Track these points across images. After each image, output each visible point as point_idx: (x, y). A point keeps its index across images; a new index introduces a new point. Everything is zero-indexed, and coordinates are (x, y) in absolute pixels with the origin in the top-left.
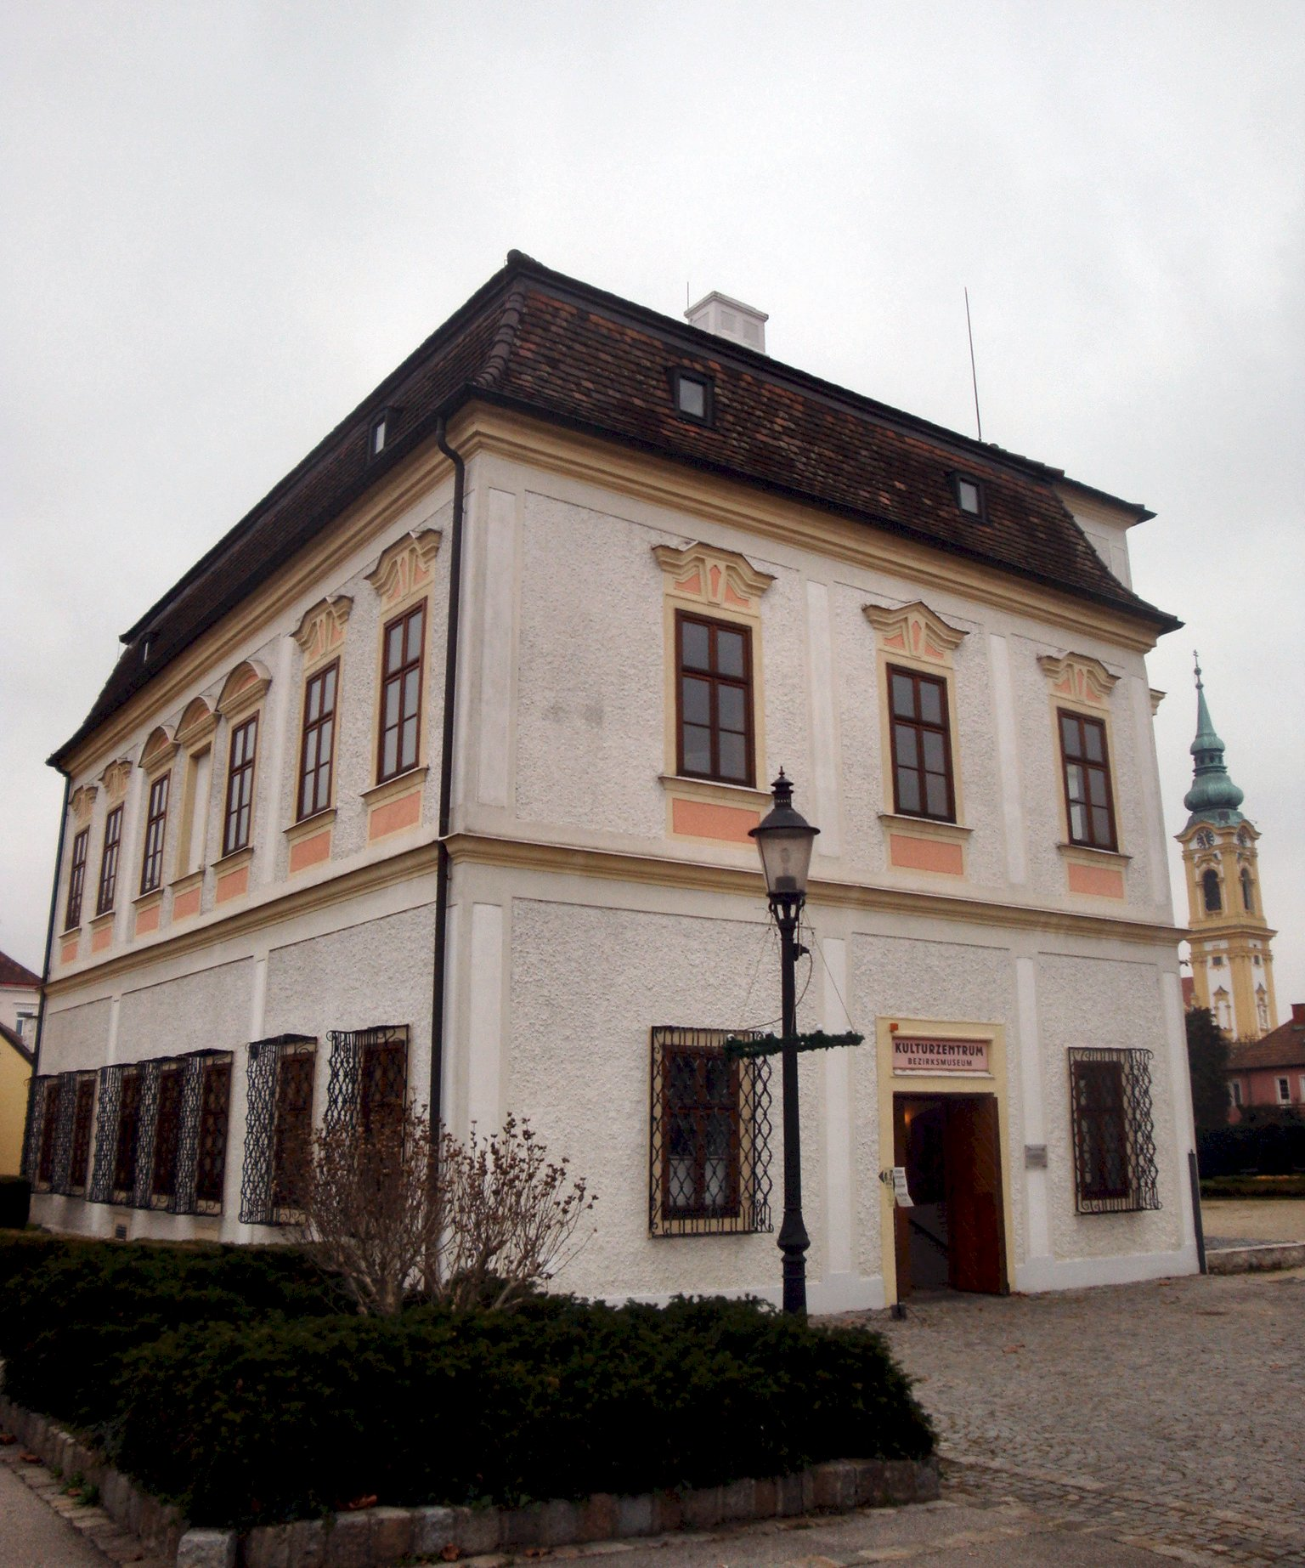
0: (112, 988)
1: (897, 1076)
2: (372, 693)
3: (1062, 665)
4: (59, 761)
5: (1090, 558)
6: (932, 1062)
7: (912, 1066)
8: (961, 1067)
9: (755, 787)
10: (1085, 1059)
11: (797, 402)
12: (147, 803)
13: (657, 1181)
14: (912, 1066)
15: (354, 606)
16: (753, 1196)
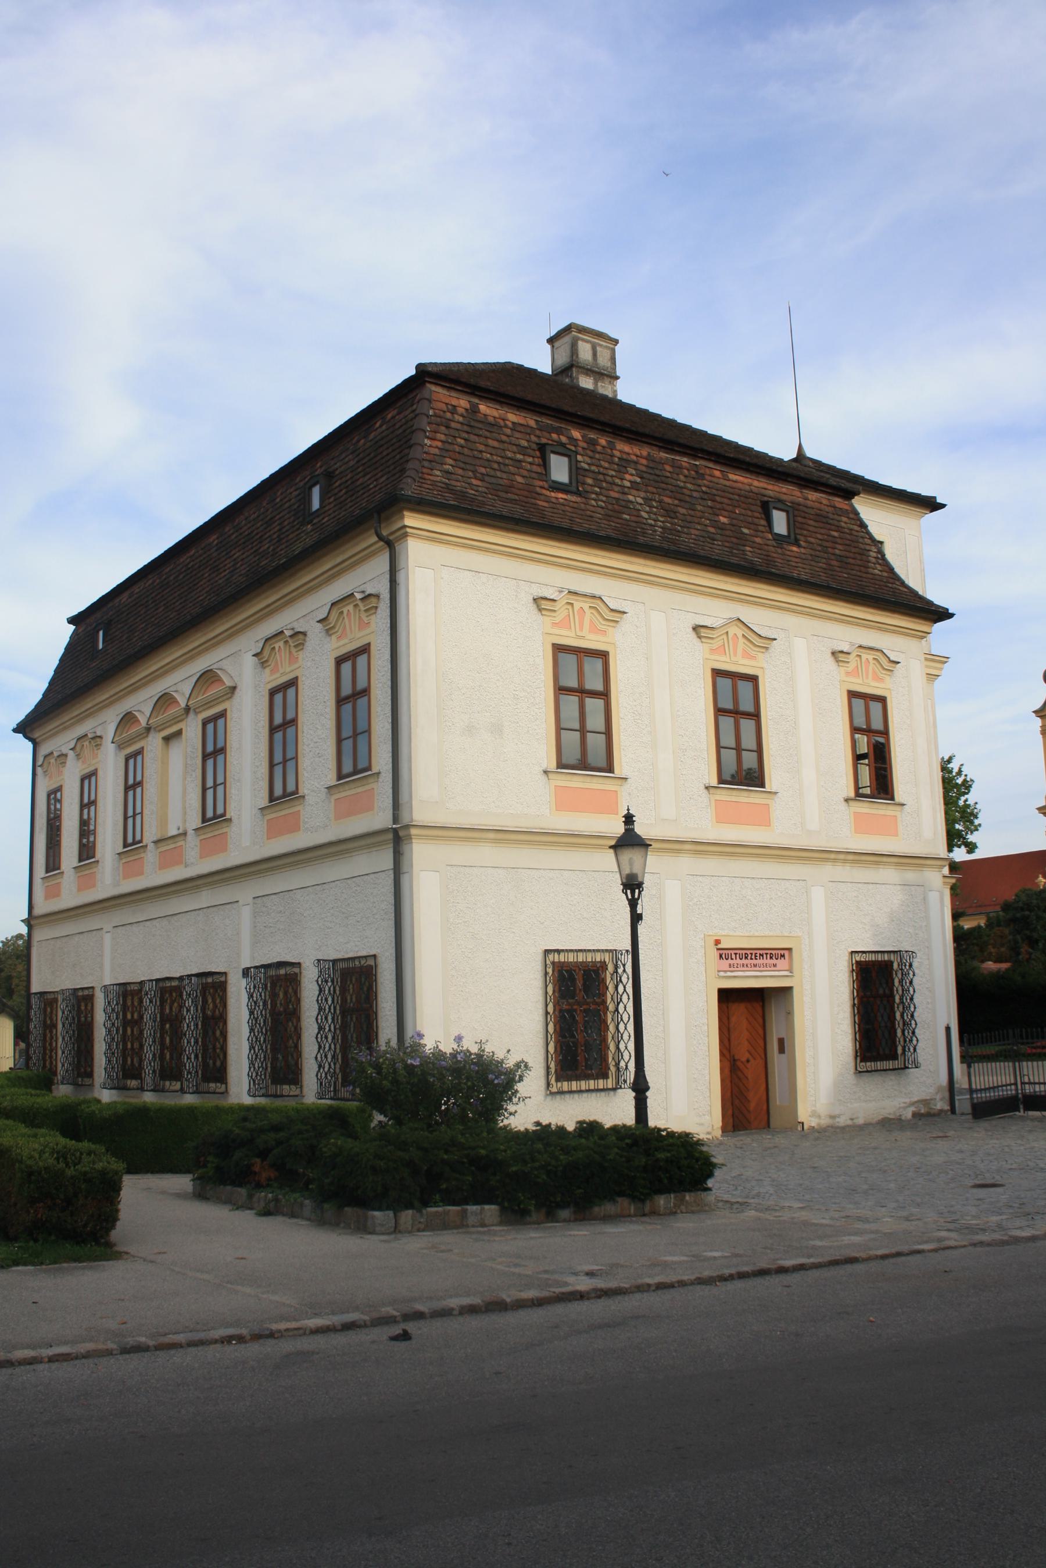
0: (104, 922)
1: (720, 977)
2: (328, 710)
3: (852, 657)
4: (24, 728)
5: (880, 561)
6: (747, 966)
7: (732, 969)
8: (769, 969)
9: (613, 773)
10: (862, 959)
11: (641, 457)
12: (122, 773)
13: (552, 1056)
14: (732, 969)
15: (307, 639)
16: (617, 1065)
